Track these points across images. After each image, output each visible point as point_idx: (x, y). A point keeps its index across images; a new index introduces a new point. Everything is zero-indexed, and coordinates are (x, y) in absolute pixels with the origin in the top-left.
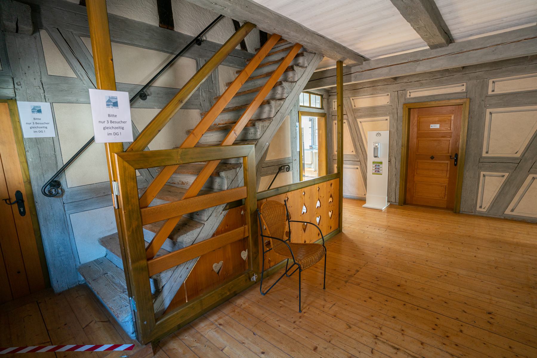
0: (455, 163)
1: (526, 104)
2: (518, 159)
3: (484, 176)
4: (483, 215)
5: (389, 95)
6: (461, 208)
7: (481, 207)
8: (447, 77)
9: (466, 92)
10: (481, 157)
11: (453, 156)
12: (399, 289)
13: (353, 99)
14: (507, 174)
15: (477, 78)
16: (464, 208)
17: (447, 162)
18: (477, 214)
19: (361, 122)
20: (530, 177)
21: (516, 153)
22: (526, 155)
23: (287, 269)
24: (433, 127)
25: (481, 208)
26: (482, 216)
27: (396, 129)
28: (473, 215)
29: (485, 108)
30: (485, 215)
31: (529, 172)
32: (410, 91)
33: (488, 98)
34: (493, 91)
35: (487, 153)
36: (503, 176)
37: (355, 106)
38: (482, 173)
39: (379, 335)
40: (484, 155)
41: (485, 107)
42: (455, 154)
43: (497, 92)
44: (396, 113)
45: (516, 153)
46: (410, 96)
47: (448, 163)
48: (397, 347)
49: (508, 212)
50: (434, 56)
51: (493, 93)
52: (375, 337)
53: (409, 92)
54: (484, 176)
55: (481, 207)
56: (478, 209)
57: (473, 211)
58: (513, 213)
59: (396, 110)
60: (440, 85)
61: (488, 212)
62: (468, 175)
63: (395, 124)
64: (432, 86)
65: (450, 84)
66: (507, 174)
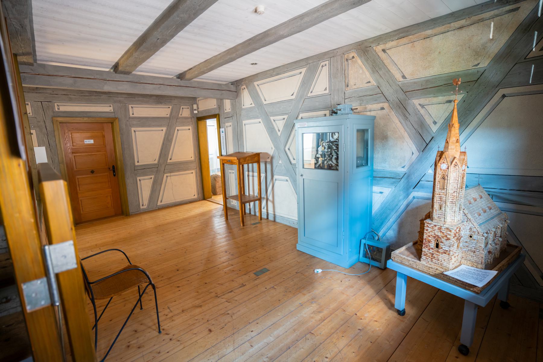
0: (114, 174)
1: (154, 126)
2: (156, 165)
3: (140, 180)
4: (145, 211)
5: (189, 108)
6: (130, 211)
7: (143, 205)
8: (95, 97)
9: (113, 113)
10: (135, 166)
11: (111, 168)
12: (179, 272)
13: (132, 107)
14: (153, 177)
15: (120, 102)
16: (132, 210)
17: (106, 174)
18: (141, 211)
19: (135, 131)
20: (165, 175)
21: (155, 160)
22: (160, 161)
23: (139, 302)
24: (87, 143)
25: (143, 206)
26: (146, 212)
27: (48, 145)
28: (141, 213)
29: (130, 127)
30: (147, 211)
31: (164, 173)
32: (58, 104)
33: (131, 119)
34: (181, 115)
35: (138, 162)
36: (151, 178)
37: (133, 114)
38: (138, 178)
39: (216, 295)
40: (137, 164)
41: (130, 126)
42: (112, 166)
43: (135, 115)
44: (44, 126)
45: (155, 160)
46: (58, 109)
47: (108, 175)
48: (230, 291)
49: (159, 203)
50: (174, 84)
51: (181, 116)
52: (217, 297)
53: (57, 105)
54: (140, 180)
55: (143, 205)
56: (141, 207)
57: (139, 210)
58: (162, 203)
59: (44, 123)
60: (90, 103)
61: (148, 207)
62: (129, 181)
63: (45, 139)
64: (83, 103)
65: (99, 103)
66: (153, 177)
